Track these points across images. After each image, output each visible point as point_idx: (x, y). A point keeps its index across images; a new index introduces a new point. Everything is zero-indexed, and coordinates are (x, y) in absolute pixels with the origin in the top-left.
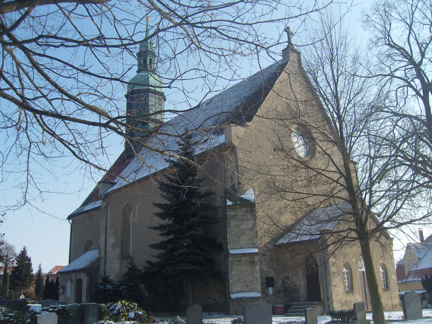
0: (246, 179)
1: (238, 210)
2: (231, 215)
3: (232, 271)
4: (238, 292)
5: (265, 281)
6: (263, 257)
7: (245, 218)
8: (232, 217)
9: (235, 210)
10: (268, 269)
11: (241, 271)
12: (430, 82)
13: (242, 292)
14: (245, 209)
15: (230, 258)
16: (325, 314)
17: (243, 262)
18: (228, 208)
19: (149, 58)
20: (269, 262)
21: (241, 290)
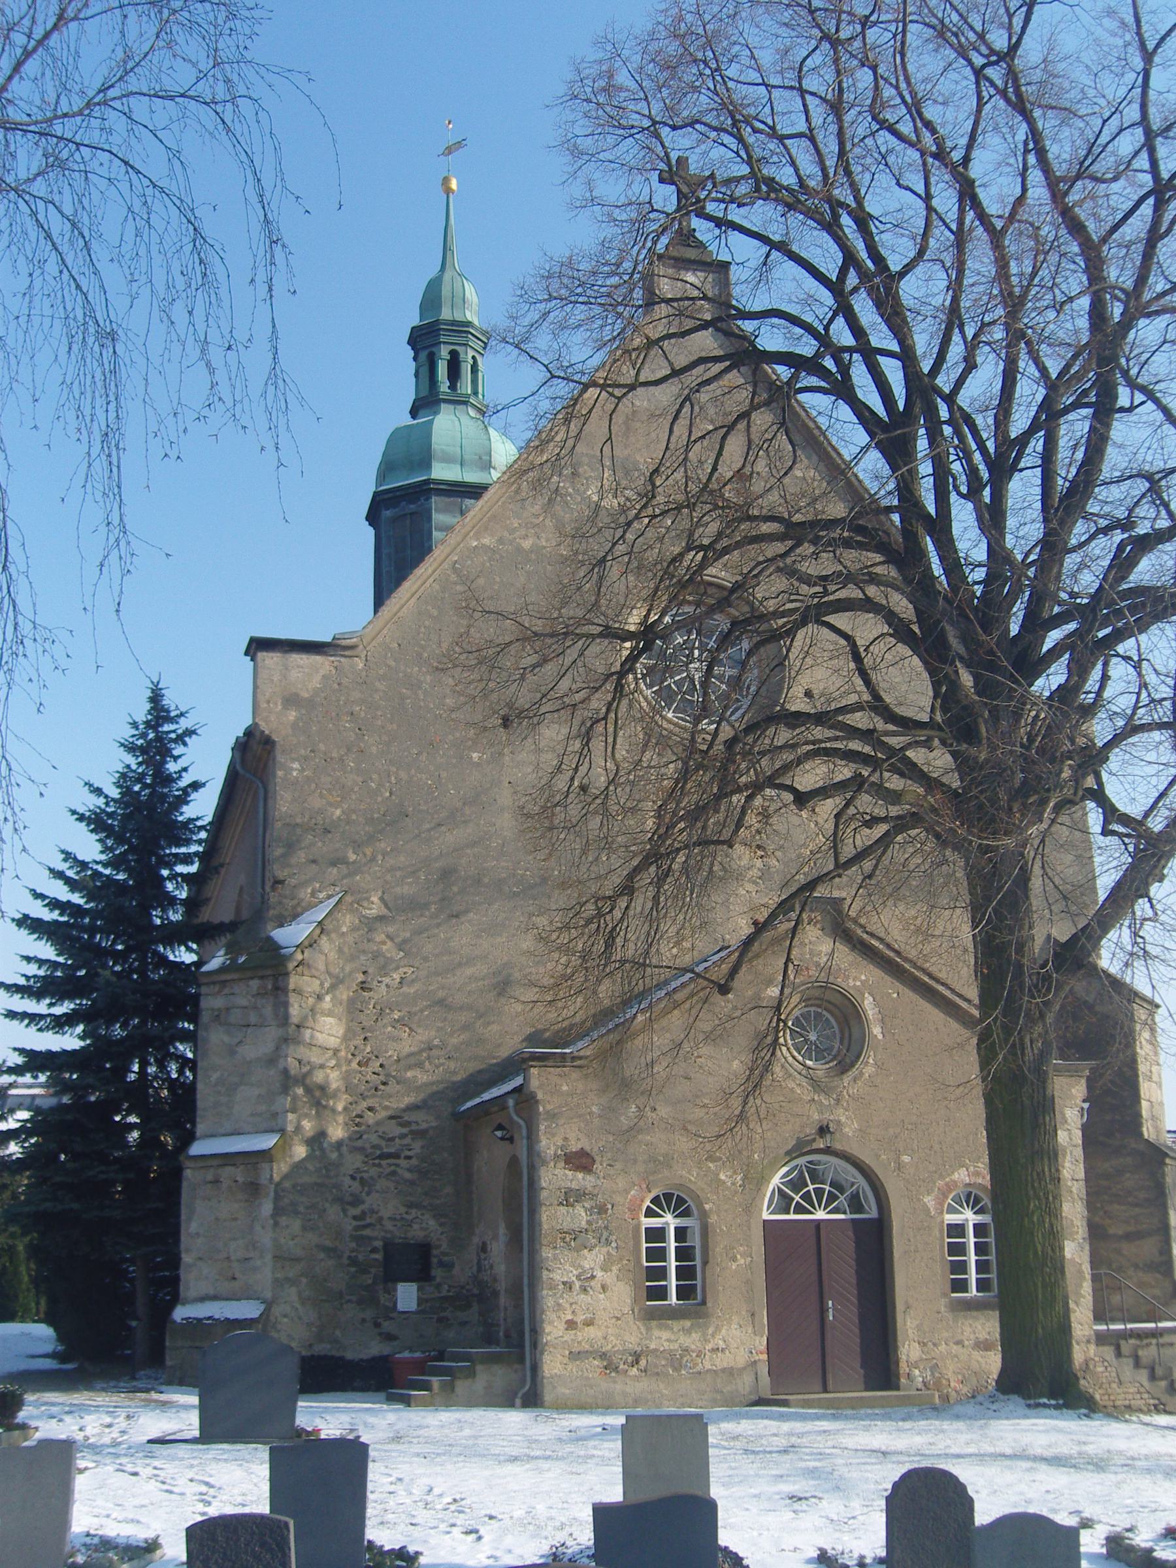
0: (314, 861)
1: (236, 989)
2: (213, 1010)
3: (189, 1220)
4: (203, 1299)
5: (379, 1256)
6: (379, 1165)
7: (253, 1018)
8: (217, 1018)
9: (226, 991)
10: (403, 1210)
11: (217, 1219)
12: (878, 357)
13: (215, 1298)
14: (255, 984)
15: (188, 1173)
16: (518, 1401)
17: (224, 1186)
18: (207, 984)
19: (444, 352)
20: (412, 1183)
21: (212, 1292)
